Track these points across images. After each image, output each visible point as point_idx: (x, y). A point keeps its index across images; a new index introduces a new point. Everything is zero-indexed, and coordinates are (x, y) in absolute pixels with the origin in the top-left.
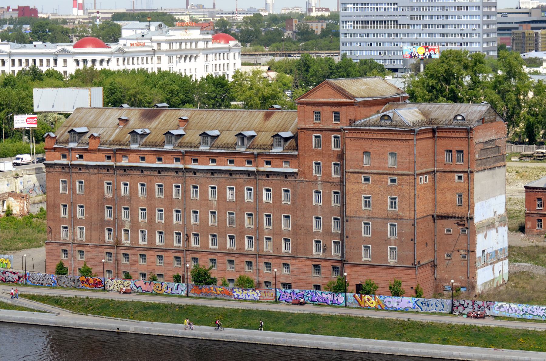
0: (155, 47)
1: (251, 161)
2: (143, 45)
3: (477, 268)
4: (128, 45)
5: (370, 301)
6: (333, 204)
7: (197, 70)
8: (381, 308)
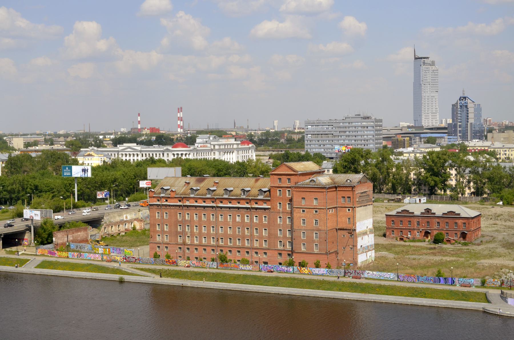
0: (212, 148)
1: (249, 204)
2: (207, 147)
3: (358, 254)
4: (199, 146)
5: (305, 270)
6: (288, 223)
7: (232, 158)
8: (310, 274)
